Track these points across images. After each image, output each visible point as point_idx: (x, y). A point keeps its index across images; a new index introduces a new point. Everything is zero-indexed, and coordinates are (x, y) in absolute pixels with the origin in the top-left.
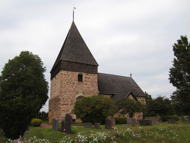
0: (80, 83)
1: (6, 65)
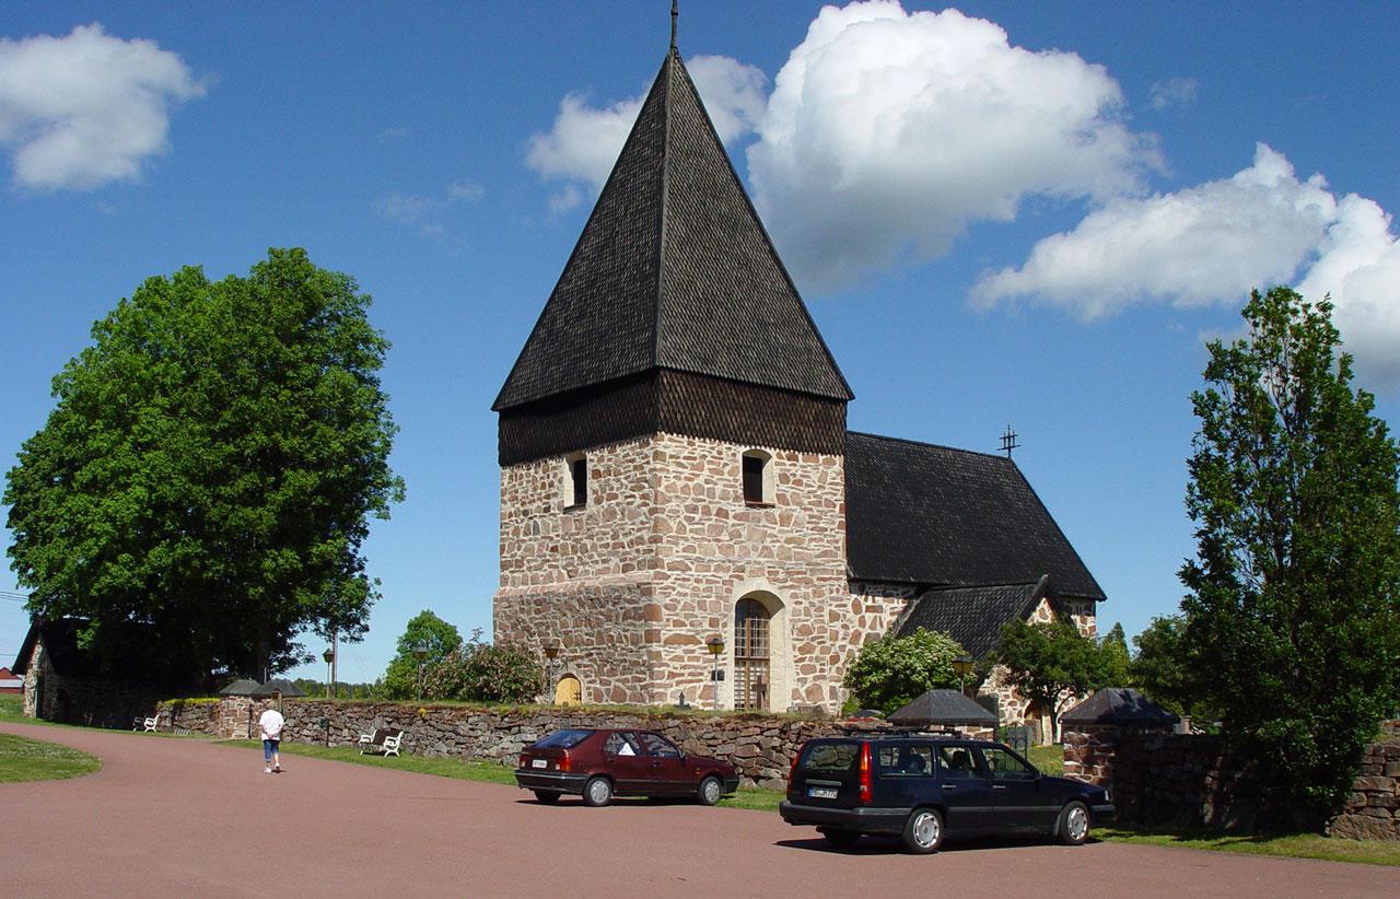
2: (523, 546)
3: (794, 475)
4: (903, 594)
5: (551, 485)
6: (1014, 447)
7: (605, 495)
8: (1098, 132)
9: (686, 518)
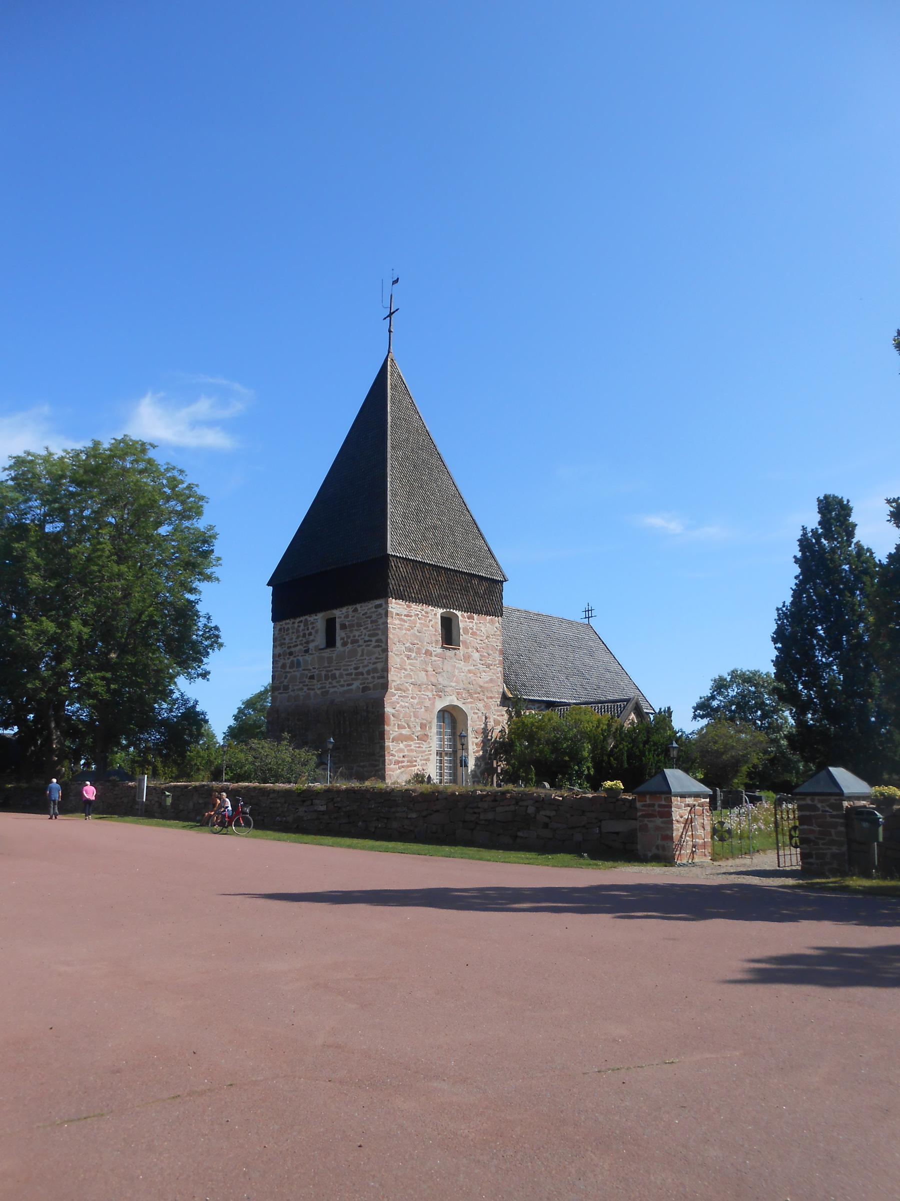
0: (450, 653)
1: (782, 615)
2: (289, 675)
3: (472, 629)
4: (538, 708)
5: (310, 634)
6: (592, 617)
7: (349, 641)
8: (278, 647)
9: (406, 655)
